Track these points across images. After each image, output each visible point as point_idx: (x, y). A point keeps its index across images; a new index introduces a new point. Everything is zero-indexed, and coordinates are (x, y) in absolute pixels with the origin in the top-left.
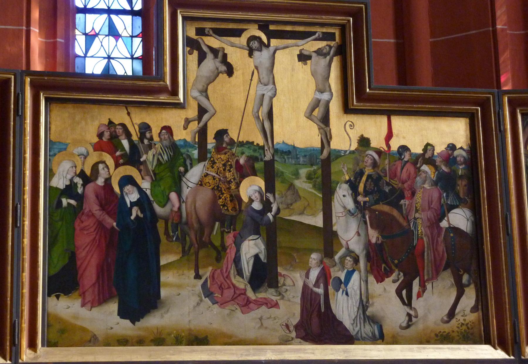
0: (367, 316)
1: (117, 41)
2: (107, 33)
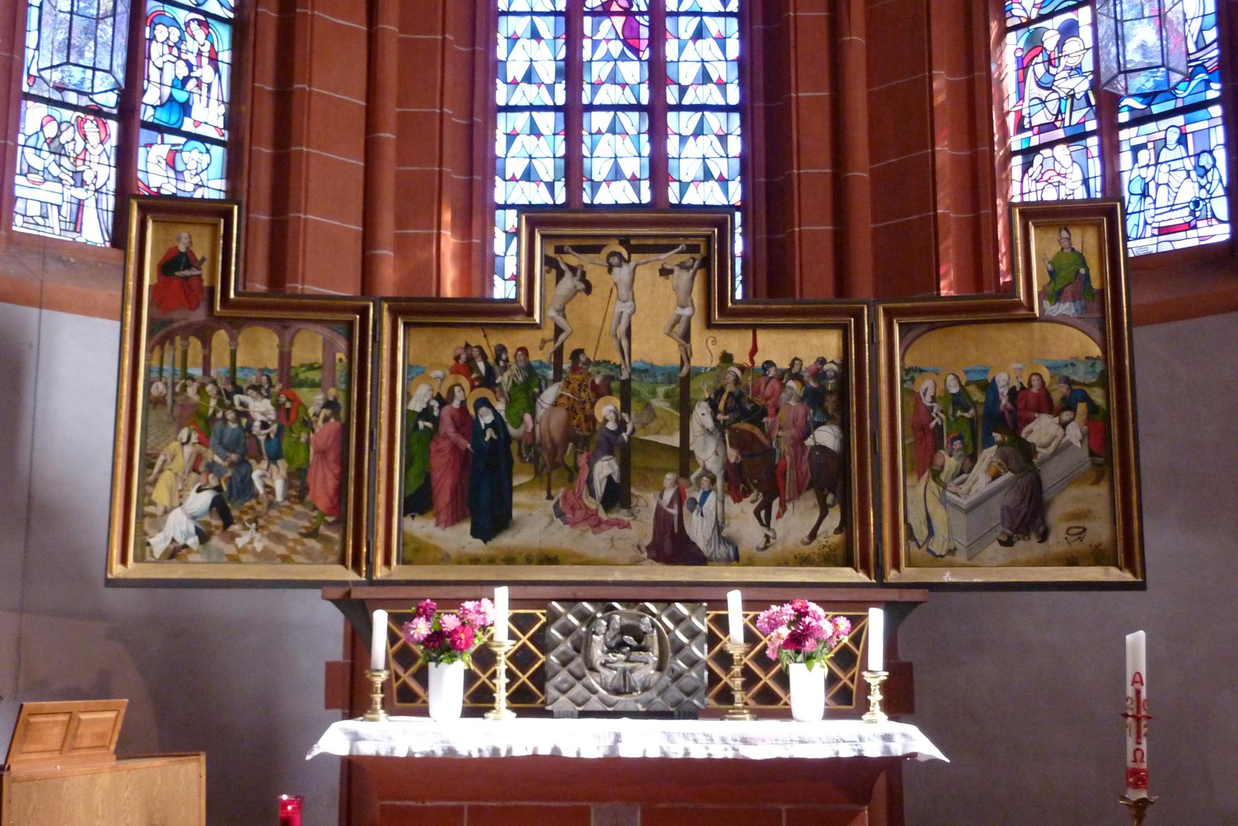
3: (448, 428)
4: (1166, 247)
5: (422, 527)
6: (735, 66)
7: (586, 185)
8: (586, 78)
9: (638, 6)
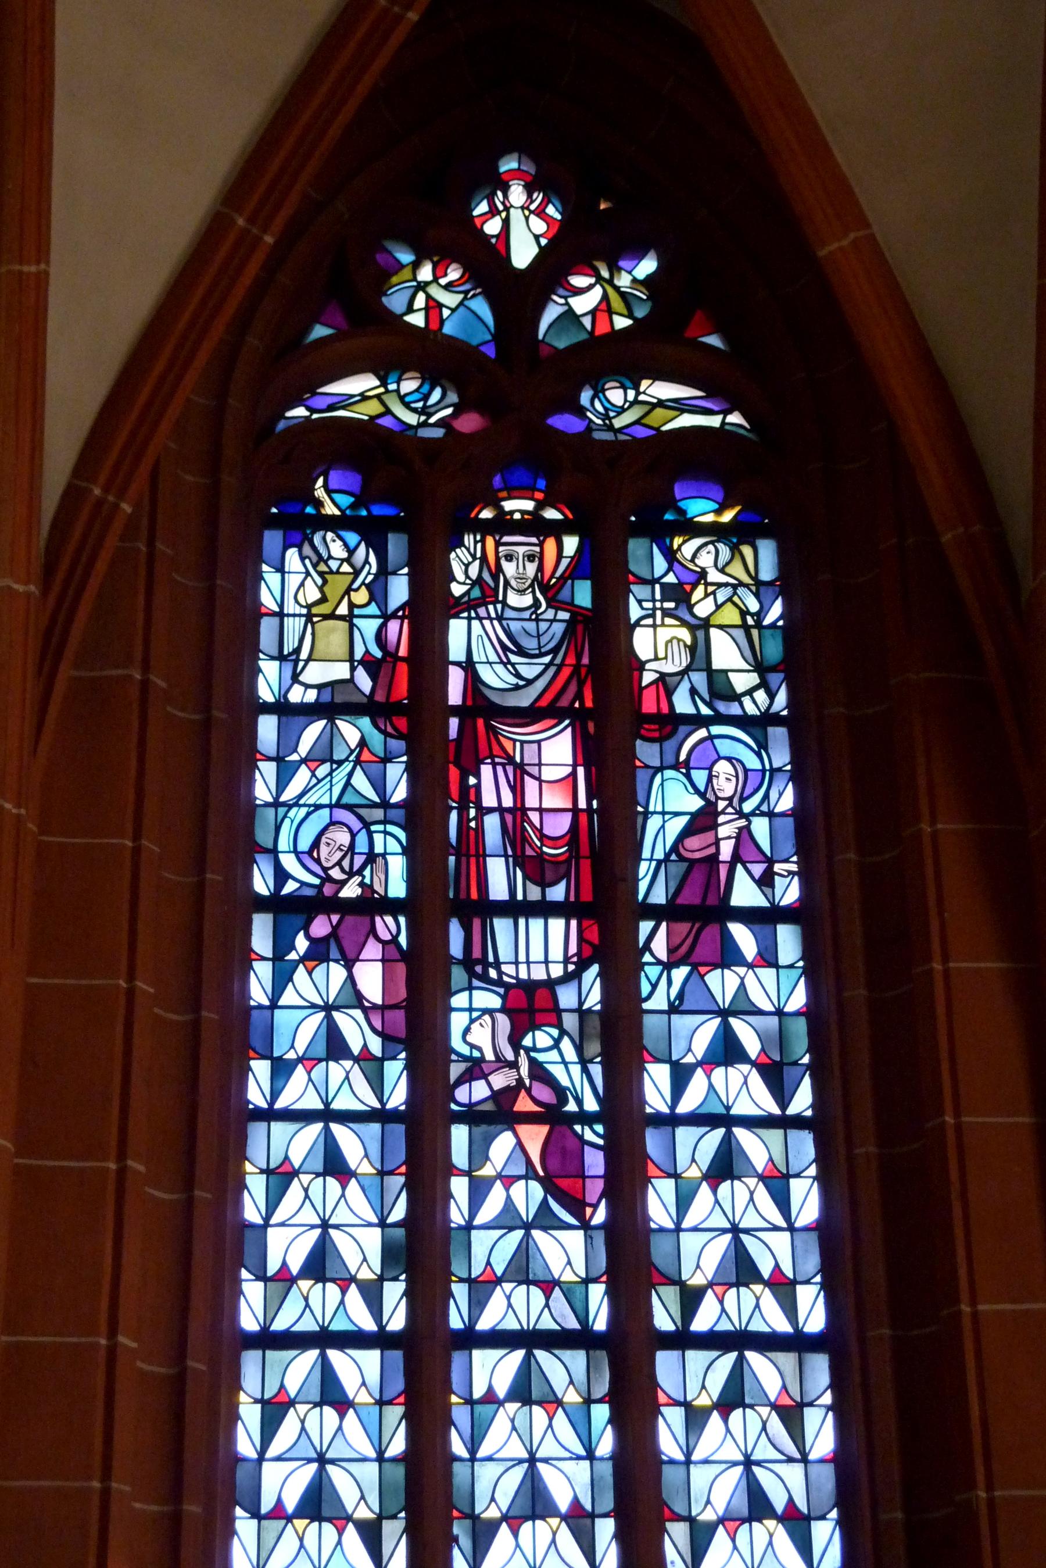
1: (344, 1186)
2: (320, 1168)
6: (812, 1241)
7: (459, 1529)
8: (458, 1268)
9: (579, 1102)
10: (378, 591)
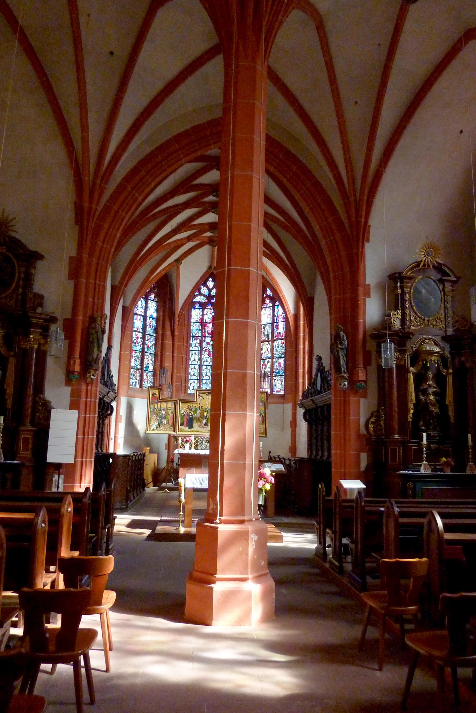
0: (379, 366)
3: (186, 415)
4: (277, 393)
5: (182, 427)
10: (200, 314)
